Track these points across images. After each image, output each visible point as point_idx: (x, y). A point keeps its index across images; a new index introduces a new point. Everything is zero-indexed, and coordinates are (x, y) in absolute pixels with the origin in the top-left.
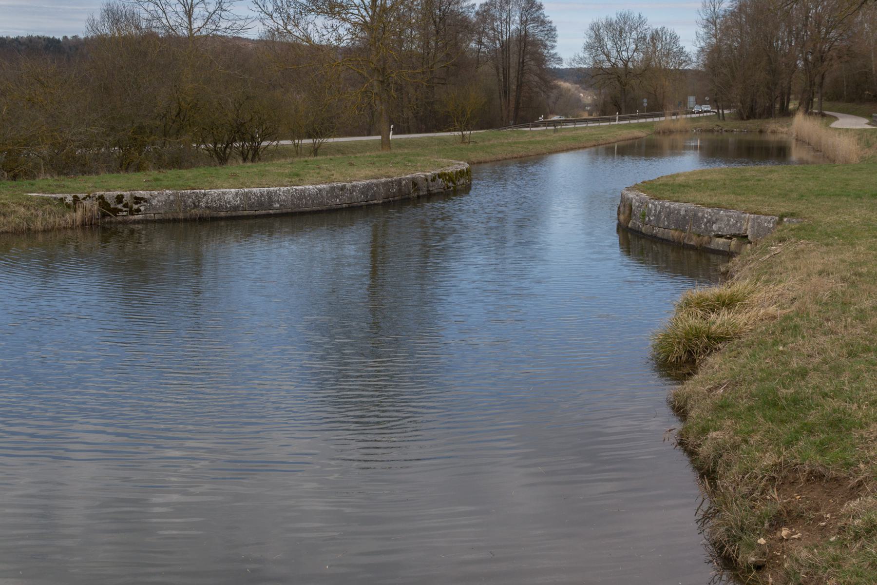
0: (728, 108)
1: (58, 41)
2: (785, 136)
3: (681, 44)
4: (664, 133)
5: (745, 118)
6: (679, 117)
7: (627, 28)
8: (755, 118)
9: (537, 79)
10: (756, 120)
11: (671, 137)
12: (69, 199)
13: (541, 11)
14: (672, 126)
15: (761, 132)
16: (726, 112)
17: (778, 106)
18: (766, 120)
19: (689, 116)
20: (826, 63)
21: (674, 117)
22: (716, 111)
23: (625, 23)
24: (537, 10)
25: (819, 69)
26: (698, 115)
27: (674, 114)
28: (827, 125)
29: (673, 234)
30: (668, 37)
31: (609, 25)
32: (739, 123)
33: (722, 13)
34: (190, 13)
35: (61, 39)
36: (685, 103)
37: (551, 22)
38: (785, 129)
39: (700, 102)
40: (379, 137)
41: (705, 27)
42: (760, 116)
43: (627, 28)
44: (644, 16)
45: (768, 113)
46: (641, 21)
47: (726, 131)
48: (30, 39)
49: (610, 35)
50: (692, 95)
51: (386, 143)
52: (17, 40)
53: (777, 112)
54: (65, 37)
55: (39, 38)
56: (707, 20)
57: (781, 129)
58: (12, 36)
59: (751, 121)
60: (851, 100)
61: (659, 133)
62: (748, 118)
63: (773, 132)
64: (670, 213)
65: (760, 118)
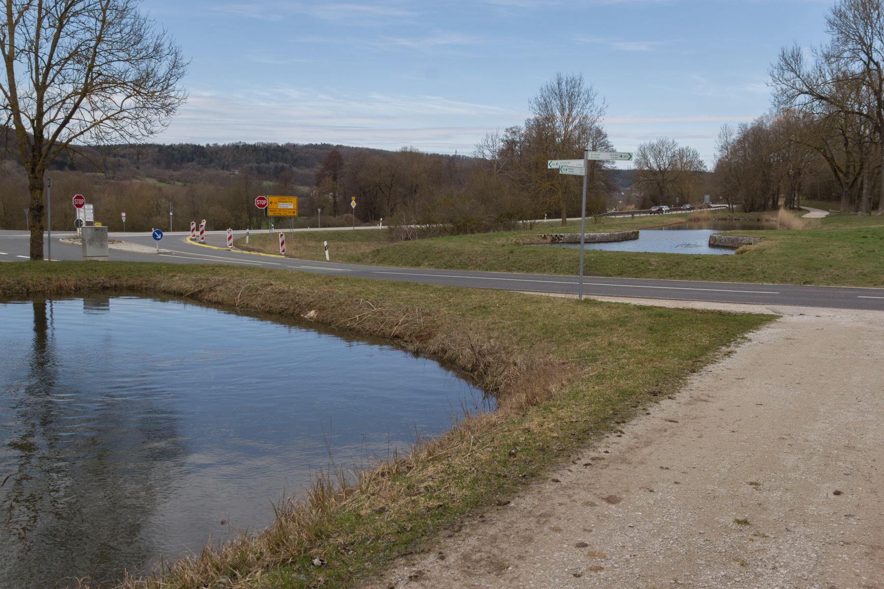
0: (735, 204)
1: (203, 147)
2: (774, 223)
3: (701, 158)
4: (695, 220)
5: (747, 210)
6: (702, 210)
7: (664, 150)
8: (754, 211)
9: (603, 184)
10: (755, 213)
11: (699, 223)
12: (543, 236)
13: (606, 139)
14: (700, 216)
15: (758, 220)
16: (734, 206)
17: (770, 203)
18: (762, 213)
19: (709, 209)
20: (802, 176)
21: (699, 210)
22: (727, 206)
23: (663, 146)
24: (603, 138)
25: (797, 180)
26: (714, 209)
27: (700, 208)
28: (800, 217)
29: (731, 244)
30: (691, 154)
31: (652, 147)
32: (743, 214)
33: (731, 141)
34: (46, 75)
35: (205, 146)
36: (701, 200)
37: (612, 146)
38: (775, 219)
39: (715, 200)
40: (561, 220)
41: (721, 151)
42: (758, 210)
43: (664, 150)
44: (676, 141)
45: (763, 208)
46: (674, 144)
47: (735, 219)
48: (181, 147)
49: (652, 154)
50: (707, 194)
51: (564, 223)
52: (171, 147)
53: (770, 207)
54: (208, 145)
55: (188, 145)
56: (722, 146)
57: (772, 218)
58: (167, 144)
59: (752, 213)
60: (823, 199)
61: (692, 220)
62: (750, 211)
63: (767, 220)
64: (729, 239)
65: (758, 211)
